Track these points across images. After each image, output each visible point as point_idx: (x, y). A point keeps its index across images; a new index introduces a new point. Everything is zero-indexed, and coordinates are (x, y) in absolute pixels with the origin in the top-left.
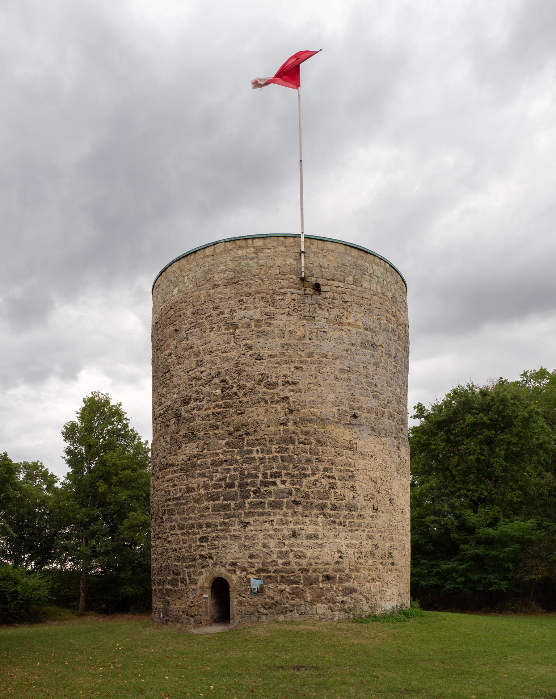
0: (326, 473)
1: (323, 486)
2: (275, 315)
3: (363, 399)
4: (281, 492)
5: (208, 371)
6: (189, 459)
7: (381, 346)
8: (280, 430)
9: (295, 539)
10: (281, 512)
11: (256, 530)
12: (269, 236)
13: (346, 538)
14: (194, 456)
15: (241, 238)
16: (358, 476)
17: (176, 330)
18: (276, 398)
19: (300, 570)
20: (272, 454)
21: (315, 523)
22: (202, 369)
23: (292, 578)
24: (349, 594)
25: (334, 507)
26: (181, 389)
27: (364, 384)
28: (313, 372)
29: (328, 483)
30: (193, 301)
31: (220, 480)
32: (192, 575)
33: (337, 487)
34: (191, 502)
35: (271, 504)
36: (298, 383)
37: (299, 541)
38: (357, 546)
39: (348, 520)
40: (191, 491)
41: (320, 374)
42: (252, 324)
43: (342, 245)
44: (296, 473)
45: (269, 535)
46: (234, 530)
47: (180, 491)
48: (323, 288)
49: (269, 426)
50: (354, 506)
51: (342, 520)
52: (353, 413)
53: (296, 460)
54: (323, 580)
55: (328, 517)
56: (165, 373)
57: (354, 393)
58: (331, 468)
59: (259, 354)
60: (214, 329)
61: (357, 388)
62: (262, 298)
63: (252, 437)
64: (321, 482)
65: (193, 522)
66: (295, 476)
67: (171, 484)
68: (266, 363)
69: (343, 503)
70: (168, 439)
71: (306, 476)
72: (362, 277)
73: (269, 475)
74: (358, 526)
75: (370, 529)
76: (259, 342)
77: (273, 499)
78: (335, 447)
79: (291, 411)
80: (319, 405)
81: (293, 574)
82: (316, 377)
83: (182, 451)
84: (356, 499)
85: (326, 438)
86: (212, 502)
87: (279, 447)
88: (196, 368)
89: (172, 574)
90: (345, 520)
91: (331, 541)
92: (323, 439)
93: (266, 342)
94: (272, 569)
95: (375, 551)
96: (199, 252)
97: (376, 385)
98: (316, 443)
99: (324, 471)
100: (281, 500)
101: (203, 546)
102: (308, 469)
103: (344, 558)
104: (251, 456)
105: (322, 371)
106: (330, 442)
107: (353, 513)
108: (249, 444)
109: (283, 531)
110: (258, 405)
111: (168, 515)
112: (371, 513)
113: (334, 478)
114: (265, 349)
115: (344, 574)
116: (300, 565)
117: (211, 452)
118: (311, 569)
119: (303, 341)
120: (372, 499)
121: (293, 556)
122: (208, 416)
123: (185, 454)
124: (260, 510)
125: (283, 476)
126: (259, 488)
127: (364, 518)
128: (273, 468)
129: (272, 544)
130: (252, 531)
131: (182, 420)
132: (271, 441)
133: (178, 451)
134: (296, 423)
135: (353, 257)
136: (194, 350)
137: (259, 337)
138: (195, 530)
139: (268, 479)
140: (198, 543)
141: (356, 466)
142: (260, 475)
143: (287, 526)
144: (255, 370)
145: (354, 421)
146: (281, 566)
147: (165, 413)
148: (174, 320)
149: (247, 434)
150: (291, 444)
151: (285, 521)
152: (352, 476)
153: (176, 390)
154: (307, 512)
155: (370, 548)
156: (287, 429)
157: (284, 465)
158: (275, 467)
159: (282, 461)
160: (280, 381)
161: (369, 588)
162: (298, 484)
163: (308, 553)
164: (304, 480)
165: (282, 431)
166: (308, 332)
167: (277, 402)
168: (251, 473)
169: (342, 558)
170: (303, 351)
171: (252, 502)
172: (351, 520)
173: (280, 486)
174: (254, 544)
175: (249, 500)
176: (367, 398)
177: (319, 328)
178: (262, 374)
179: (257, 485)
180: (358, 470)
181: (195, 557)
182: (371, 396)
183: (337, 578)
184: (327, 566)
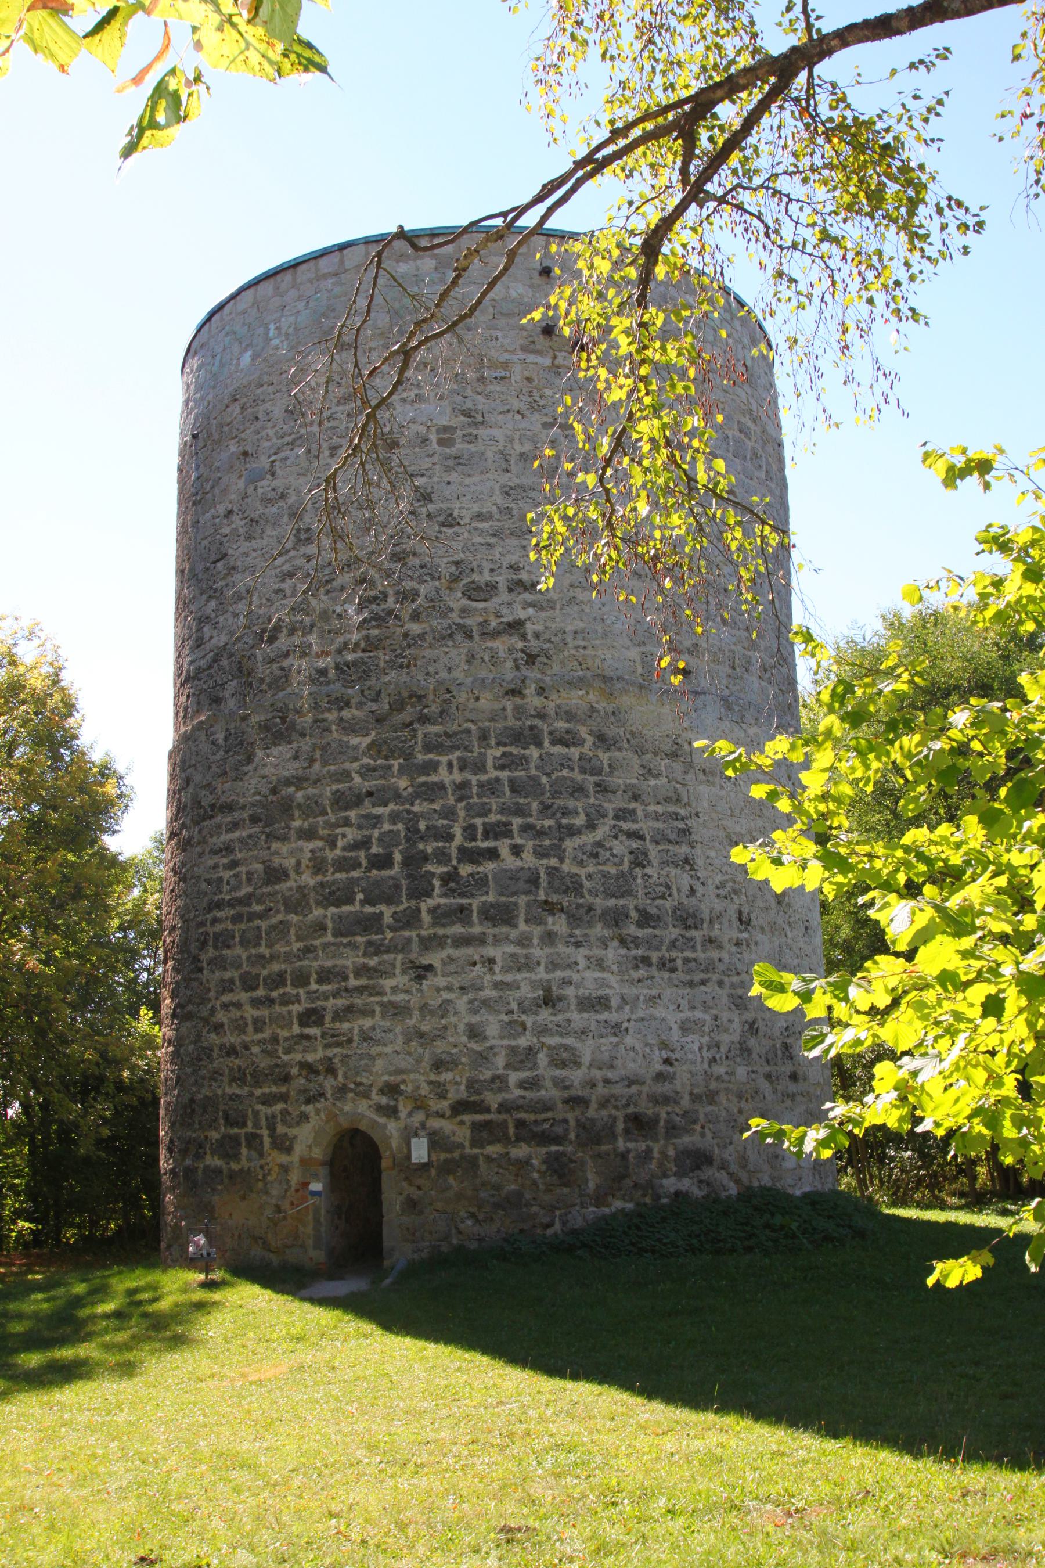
0: (621, 823)
1: (616, 860)
4: (511, 879)
9: (551, 1010)
10: (514, 934)
11: (449, 988)
18: (493, 624)
19: (566, 1101)
21: (600, 964)
23: (546, 1126)
24: (692, 1171)
25: (646, 919)
29: (626, 851)
31: (356, 846)
33: (649, 862)
37: (560, 1018)
38: (706, 1029)
40: (278, 880)
42: (433, 437)
44: (547, 823)
47: (249, 880)
50: (694, 916)
55: (632, 945)
56: (214, 562)
64: (611, 849)
67: (225, 861)
68: (466, 534)
69: (668, 904)
71: (572, 832)
73: (480, 830)
74: (706, 971)
75: (735, 979)
76: (449, 483)
77: (491, 898)
78: (640, 751)
81: (549, 1114)
83: (255, 769)
84: (698, 895)
85: (617, 730)
87: (504, 754)
89: (222, 1121)
90: (674, 954)
91: (641, 1014)
94: (493, 1100)
95: (752, 1042)
99: (617, 817)
101: (308, 1037)
102: (577, 813)
104: (434, 778)
107: (693, 933)
108: (428, 748)
109: (518, 988)
113: (642, 838)
115: (677, 1110)
116: (566, 1088)
118: (594, 1098)
124: (457, 929)
127: (720, 947)
132: (484, 737)
137: (448, 469)
140: (296, 1029)
141: (694, 805)
142: (457, 831)
143: (528, 975)
146: (518, 1092)
147: (210, 667)
148: (241, 428)
150: (532, 747)
151: (523, 960)
154: (577, 932)
157: (517, 803)
158: (494, 807)
160: (502, 580)
163: (586, 1051)
164: (569, 844)
165: (509, 712)
167: (495, 634)
169: (671, 1065)
172: (689, 954)
178: (457, 563)
179: (450, 860)
180: (697, 815)
183: (662, 1123)
184: (634, 1089)
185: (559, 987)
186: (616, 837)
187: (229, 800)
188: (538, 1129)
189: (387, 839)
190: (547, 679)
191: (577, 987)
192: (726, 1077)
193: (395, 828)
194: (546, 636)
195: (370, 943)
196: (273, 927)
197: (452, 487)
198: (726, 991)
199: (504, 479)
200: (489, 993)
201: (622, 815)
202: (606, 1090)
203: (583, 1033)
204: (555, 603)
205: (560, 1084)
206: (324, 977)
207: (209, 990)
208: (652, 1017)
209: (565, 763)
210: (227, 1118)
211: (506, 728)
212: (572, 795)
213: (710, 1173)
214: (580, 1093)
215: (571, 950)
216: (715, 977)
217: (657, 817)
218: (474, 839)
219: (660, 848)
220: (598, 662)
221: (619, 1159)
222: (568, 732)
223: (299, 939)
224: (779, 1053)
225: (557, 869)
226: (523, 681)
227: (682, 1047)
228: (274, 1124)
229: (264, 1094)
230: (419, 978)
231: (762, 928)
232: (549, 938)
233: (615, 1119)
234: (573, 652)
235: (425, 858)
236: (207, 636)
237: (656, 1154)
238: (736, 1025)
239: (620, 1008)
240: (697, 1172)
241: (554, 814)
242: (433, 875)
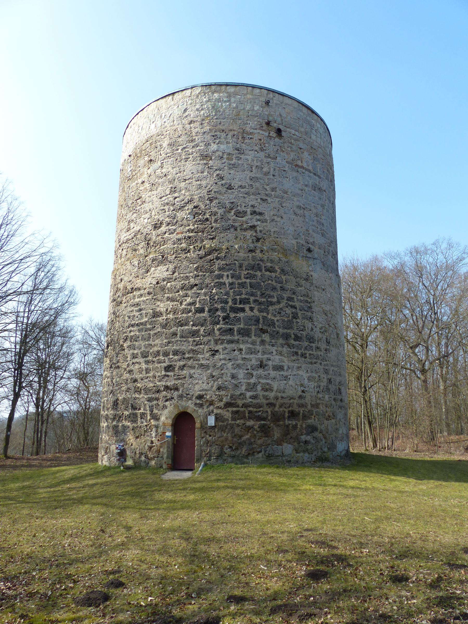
0: (289, 302)
1: (287, 315)
2: (245, 151)
3: (315, 235)
4: (249, 319)
5: (182, 197)
6: (158, 283)
7: (325, 191)
8: (248, 257)
9: (262, 370)
10: (250, 340)
11: (225, 359)
16: (315, 309)
19: (267, 404)
20: (241, 279)
21: (281, 354)
22: (176, 195)
23: (260, 414)
24: (311, 433)
25: (297, 338)
26: (152, 214)
31: (190, 304)
34: (158, 328)
36: (264, 213)
37: (266, 373)
38: (316, 380)
39: (308, 352)
40: (158, 316)
42: (225, 156)
44: (263, 300)
45: (238, 365)
46: (202, 358)
47: (146, 316)
48: (283, 134)
50: (313, 338)
54: (289, 417)
56: (136, 200)
60: (189, 160)
63: (224, 262)
65: (159, 349)
67: (137, 309)
68: (236, 193)
69: (304, 333)
70: (136, 263)
71: (272, 304)
72: (311, 131)
73: (238, 301)
74: (316, 359)
75: (325, 363)
77: (242, 326)
79: (258, 240)
80: (282, 236)
81: (261, 409)
82: (278, 210)
83: (151, 274)
84: (314, 331)
85: (288, 268)
86: (180, 328)
87: (248, 273)
89: (130, 408)
90: (306, 352)
91: (295, 373)
93: (237, 173)
94: (240, 403)
95: (330, 386)
99: (288, 300)
100: (250, 327)
101: (168, 376)
102: (274, 297)
104: (221, 280)
105: (284, 205)
107: (312, 344)
108: (220, 269)
109: (251, 360)
110: (229, 232)
111: (131, 341)
112: (325, 346)
115: (306, 410)
116: (267, 399)
117: (182, 275)
118: (277, 403)
119: (268, 177)
121: (261, 388)
122: (179, 240)
124: (229, 337)
125: (251, 302)
126: (229, 314)
127: (321, 351)
128: (242, 293)
129: (241, 374)
130: (220, 360)
132: (241, 266)
133: (146, 275)
134: (262, 251)
135: (304, 114)
137: (230, 168)
139: (238, 305)
140: (163, 373)
141: (313, 298)
142: (230, 300)
143: (255, 356)
144: (226, 199)
145: (309, 255)
146: (251, 400)
147: (133, 238)
148: (150, 151)
149: (218, 258)
151: (253, 350)
154: (273, 341)
155: (326, 383)
156: (255, 256)
157: (252, 292)
158: (244, 292)
159: (251, 287)
160: (249, 210)
162: (265, 312)
163: (275, 386)
164: (270, 308)
165: (250, 258)
166: (272, 169)
167: (246, 230)
169: (304, 393)
170: (268, 185)
172: (311, 352)
173: (248, 313)
174: (223, 374)
175: (218, 326)
178: (232, 203)
179: (226, 311)
180: (314, 302)
181: (159, 388)
182: (321, 234)
183: (301, 414)
184: (292, 401)
185: (266, 361)
186: (287, 307)
188: (257, 414)
190: (265, 248)
192: (322, 399)
194: (264, 232)
195: (194, 341)
196: (155, 334)
198: (322, 367)
200: (240, 362)
201: (290, 299)
203: (274, 379)
204: (267, 220)
205: (266, 398)
207: (127, 357)
208: (298, 374)
209: (270, 278)
210: (132, 406)
212: (272, 290)
213: (317, 434)
215: (270, 347)
216: (319, 361)
217: (301, 301)
218: (236, 304)
220: (282, 243)
221: (286, 427)
222: (271, 267)
223: (166, 338)
226: (255, 247)
228: (152, 409)
229: (149, 397)
230: (213, 355)
231: (333, 345)
232: (263, 342)
234: (274, 239)
236: (132, 227)
237: (299, 426)
238: (325, 380)
239: (287, 370)
240: (313, 434)
241: (265, 297)
242: (219, 316)
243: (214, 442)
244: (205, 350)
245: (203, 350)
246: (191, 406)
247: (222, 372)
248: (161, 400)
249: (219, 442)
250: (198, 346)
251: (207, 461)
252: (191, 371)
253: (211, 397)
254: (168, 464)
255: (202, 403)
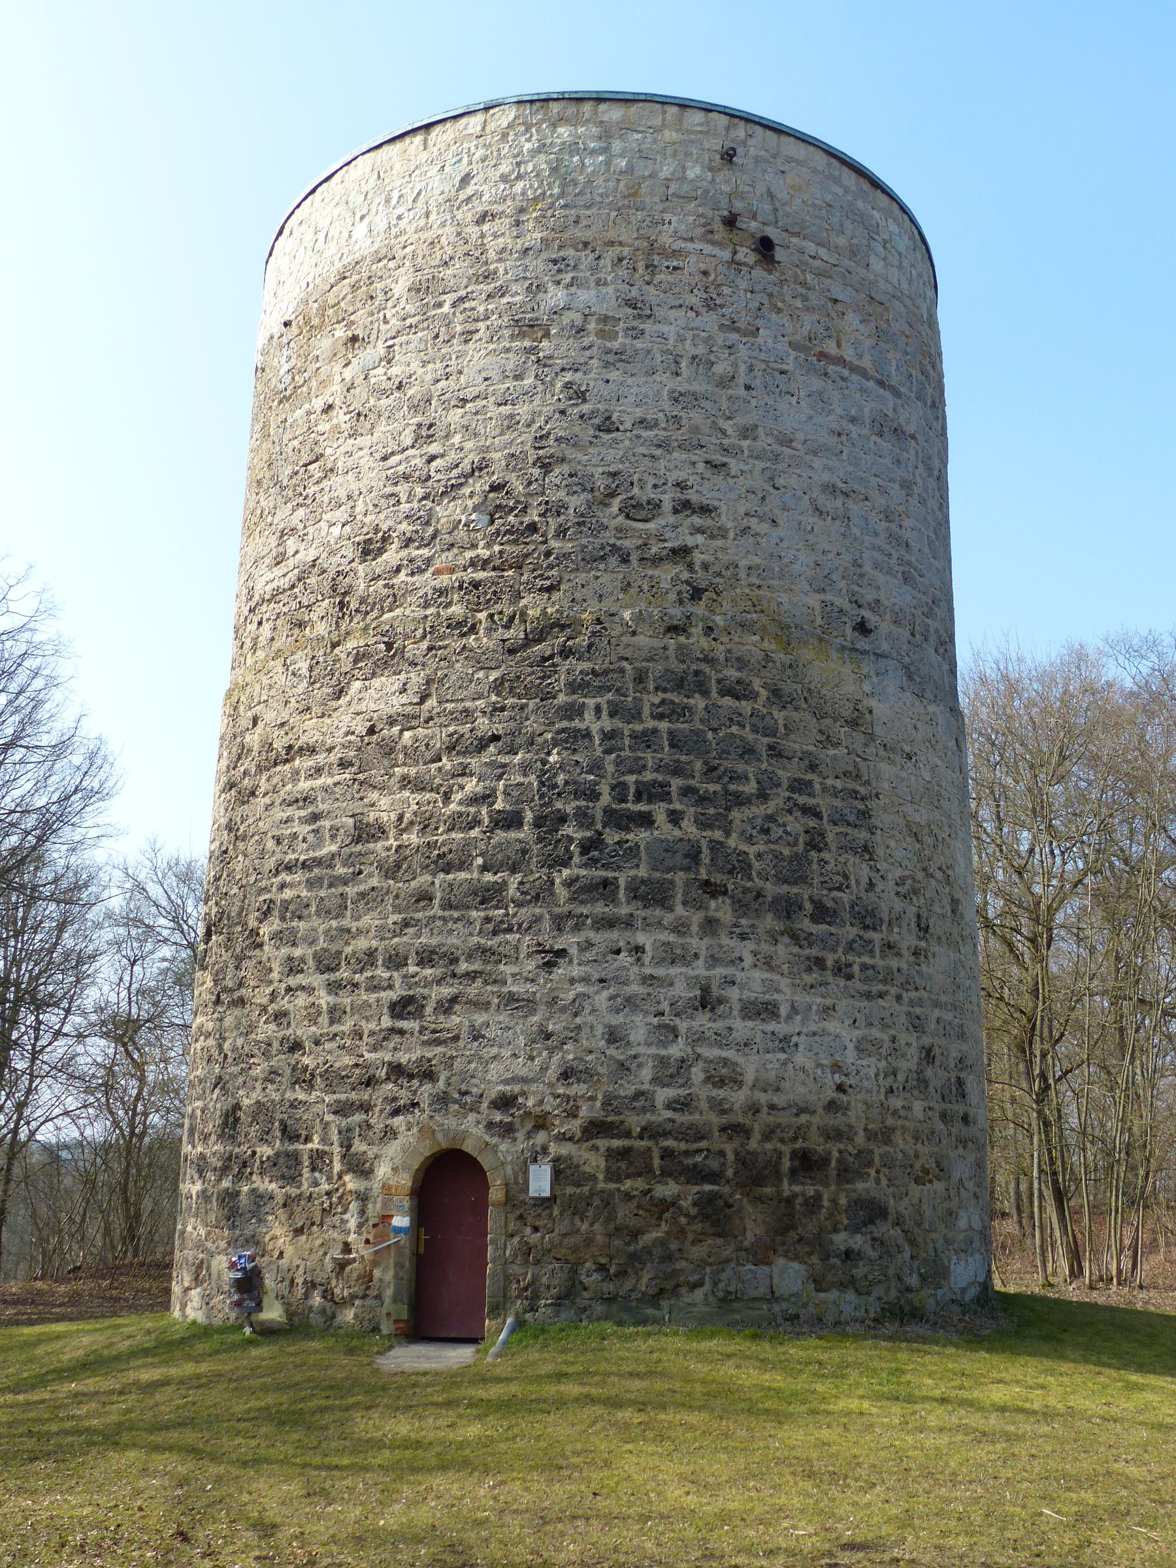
0: (796, 796)
1: (790, 839)
2: (655, 308)
3: (881, 578)
4: (667, 851)
5: (452, 457)
6: (371, 731)
7: (913, 437)
8: (665, 648)
9: (708, 1015)
10: (668, 918)
11: (585, 980)
12: (643, 97)
13: (855, 1022)
14: (392, 722)
15: (567, 96)
16: (882, 818)
17: (354, 339)
18: (654, 550)
19: (723, 1129)
21: (768, 964)
22: (434, 448)
23: (699, 1159)
24: (865, 1225)
25: (821, 913)
26: (357, 510)
27: (883, 536)
28: (757, 481)
29: (802, 829)
30: (414, 255)
31: (475, 800)
32: (356, 1141)
33: (826, 845)
34: (370, 875)
35: (636, 889)
36: (716, 509)
37: (719, 1025)
38: (883, 1051)
39: (857, 960)
40: (373, 838)
41: (775, 492)
42: (592, 326)
43: (821, 152)
44: (712, 787)
47: (333, 837)
48: (779, 254)
49: (634, 633)
50: (872, 914)
51: (843, 958)
52: (859, 620)
53: (714, 745)
54: (793, 1172)
55: (805, 943)
56: (306, 465)
57: (861, 558)
58: (810, 782)
59: (607, 414)
60: (476, 336)
61: (866, 544)
62: (620, 260)
63: (586, 666)
64: (785, 826)
65: (374, 943)
66: (711, 801)
67: (303, 813)
68: (627, 443)
69: (845, 897)
70: (303, 666)
71: (740, 800)
72: (868, 246)
73: (632, 790)
74: (884, 981)
76: (608, 381)
77: (643, 872)
78: (819, 714)
79: (697, 594)
81: (703, 1144)
82: (763, 498)
84: (878, 889)
85: (795, 686)
86: (442, 875)
87: (663, 702)
88: (413, 447)
89: (279, 1134)
90: (851, 958)
91: (813, 1027)
92: (788, 687)
94: (635, 1122)
95: (929, 1073)
96: (438, 129)
97: (907, 545)
98: (768, 699)
99: (792, 789)
101: (401, 1032)
102: (747, 778)
103: (850, 1090)
104: (576, 724)
105: (780, 482)
106: (805, 699)
108: (573, 687)
109: (671, 985)
111: (283, 919)
113: (818, 815)
114: (626, 401)
115: (850, 1148)
116: (723, 1112)
117: (450, 706)
118: (756, 1127)
119: (730, 392)
120: (915, 893)
121: (702, 1076)
122: (442, 592)
123: (358, 714)
124: (600, 908)
125: (674, 795)
126: (600, 834)
127: (899, 955)
129: (639, 1028)
130: (572, 981)
131: (353, 606)
134: (710, 629)
136: (410, 393)
137: (607, 365)
138: (378, 972)
139: (629, 805)
140: (387, 1022)
141: (874, 783)
142: (605, 789)
143: (683, 970)
144: (594, 461)
145: (862, 643)
146: (669, 1114)
147: (293, 587)
148: (351, 309)
149: (565, 653)
150: (697, 695)
151: (678, 951)
152: (863, 813)
153: (341, 514)
154: (744, 922)
155: (916, 1060)
156: (686, 647)
157: (678, 761)
159: (672, 746)
161: (915, 1201)
164: (736, 815)
165: (671, 652)
166: (743, 368)
167: (657, 561)
168: (575, 783)
170: (729, 418)
171: (577, 878)
172: (866, 959)
173: (664, 829)
175: (566, 872)
176: (889, 578)
177: (772, 359)
178: (614, 475)
179: (593, 823)
180: (877, 796)
182: (900, 575)
183: (833, 1164)
184: (804, 1118)
186: (790, 812)
187: (311, 741)
189: (515, 793)
191: (741, 989)
192: (902, 1113)
193: (527, 780)
194: (716, 568)
195: (488, 920)
197: (612, 386)
199: (672, 383)
200: (635, 988)
201: (800, 785)
202: (771, 1119)
203: (746, 1045)
204: (727, 531)
205: (719, 1107)
206: (427, 957)
207: (271, 970)
208: (824, 1033)
209: (735, 718)
210: (284, 1129)
211: (667, 670)
212: (741, 756)
214: (741, 1120)
215: (734, 943)
218: (624, 800)
219: (838, 829)
221: (783, 1204)
224: (954, 1088)
225: (721, 843)
226: (688, 617)
227: (858, 1072)
229: (338, 1101)
230: (550, 965)
233: (780, 1154)
234: (747, 591)
235: (563, 819)
236: (290, 552)
237: (826, 1203)
238: (913, 1051)
239: (789, 1018)
240: (871, 1228)
241: (720, 778)
243: (550, 1251)
244: (524, 951)
245: (517, 948)
246: (474, 1130)
247: (578, 1020)
248: (377, 1109)
249: (563, 1251)
250: (501, 938)
251: (526, 1311)
252: (476, 1016)
253: (541, 1102)
254: (396, 1322)
255: (511, 1123)
